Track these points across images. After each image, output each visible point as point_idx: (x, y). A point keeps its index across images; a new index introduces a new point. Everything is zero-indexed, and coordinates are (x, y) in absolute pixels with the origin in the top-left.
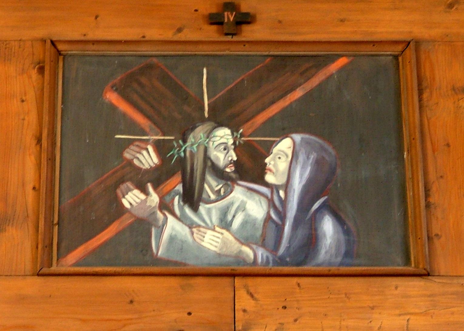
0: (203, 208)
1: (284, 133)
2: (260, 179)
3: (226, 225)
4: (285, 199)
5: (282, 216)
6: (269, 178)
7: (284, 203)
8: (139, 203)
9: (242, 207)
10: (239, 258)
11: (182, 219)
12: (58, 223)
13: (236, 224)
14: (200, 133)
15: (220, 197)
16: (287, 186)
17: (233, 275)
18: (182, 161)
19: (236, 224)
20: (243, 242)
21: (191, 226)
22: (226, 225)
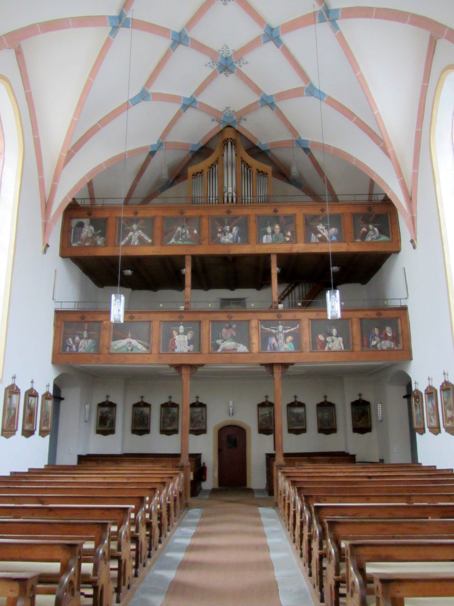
0: (226, 236)
1: (234, 226)
2: (232, 232)
3: (228, 238)
4: (240, 125)
5: (234, 237)
6: (233, 232)
7: (234, 235)
8: (270, 338)
9: (230, 236)
10: (230, 243)
11: (224, 237)
12: (408, 498)
13: (229, 238)
14: (225, 227)
15: (228, 235)
16: (235, 233)
17: (229, 245)
18: (224, 230)
19: (229, 238)
20: (225, 202)
21: (225, 238)
22: (228, 238)
